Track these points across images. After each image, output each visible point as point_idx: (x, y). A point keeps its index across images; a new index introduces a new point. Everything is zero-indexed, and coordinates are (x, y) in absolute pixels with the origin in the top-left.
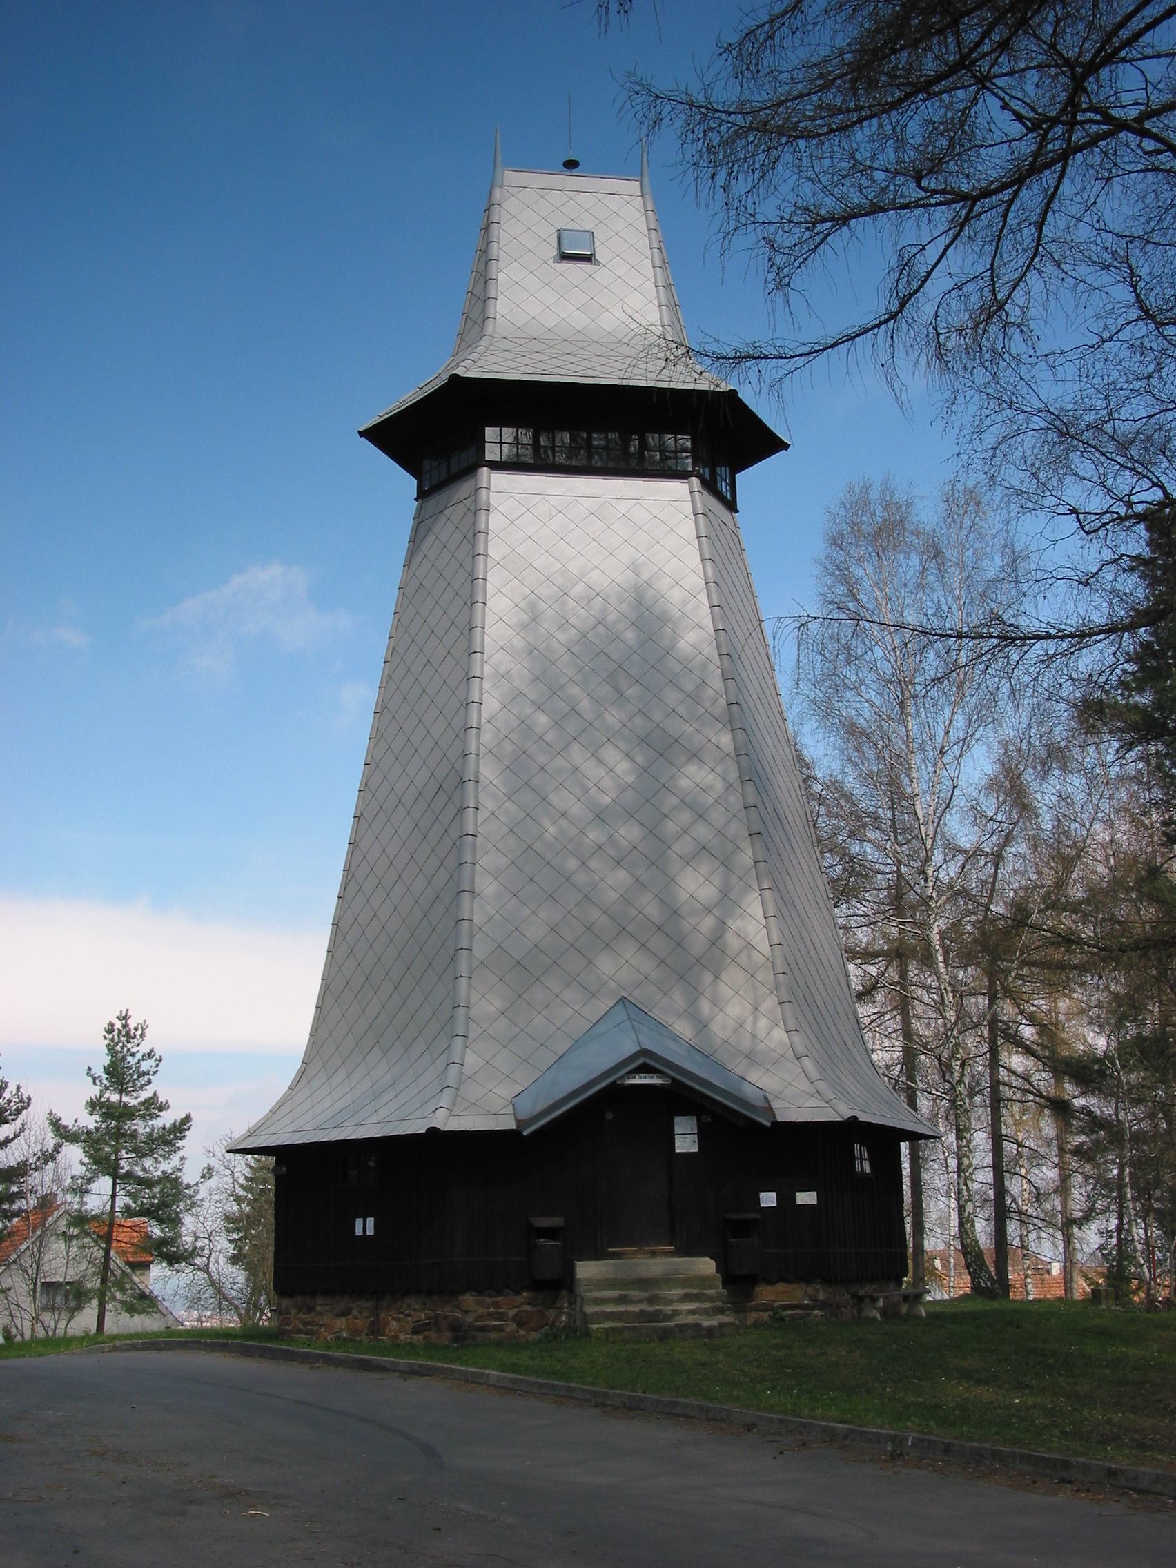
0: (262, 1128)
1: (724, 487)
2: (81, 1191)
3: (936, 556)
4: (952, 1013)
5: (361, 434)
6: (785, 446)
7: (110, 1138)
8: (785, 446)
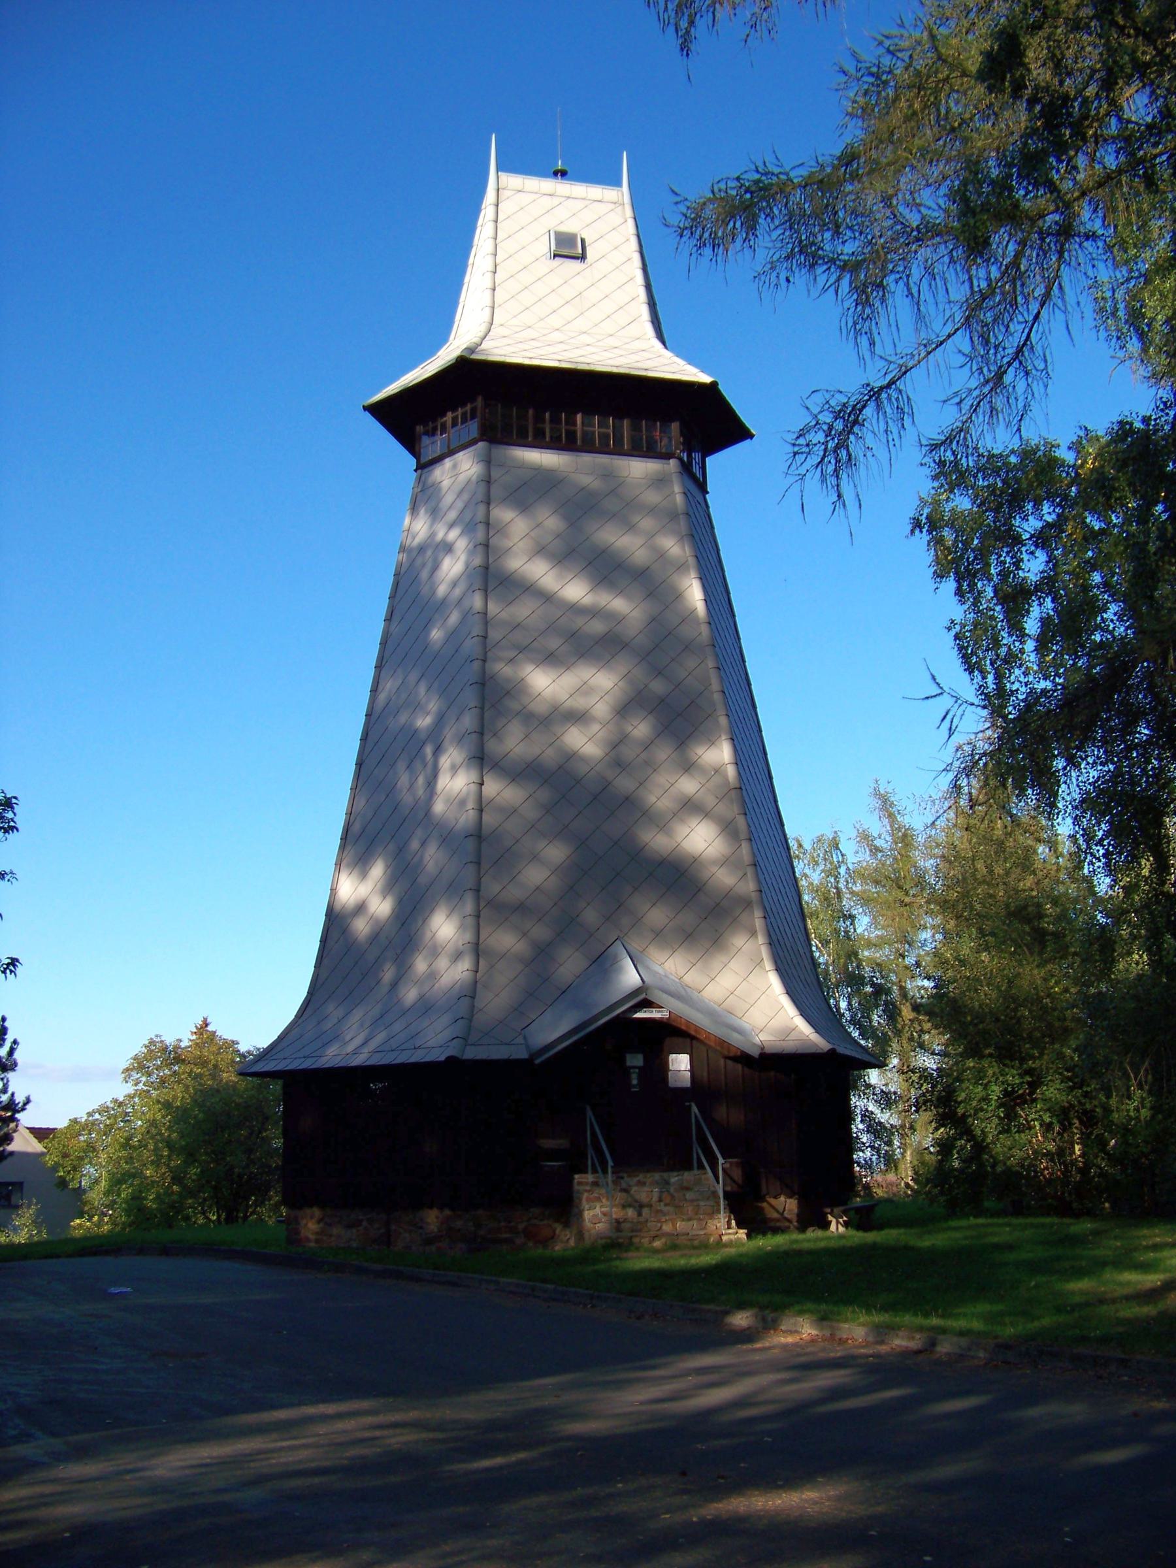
0: (269, 1055)
1: (696, 470)
2: (984, 585)
3: (94, 1150)
4: (821, 960)
5: (365, 408)
6: (751, 436)
7: (1083, 835)
8: (751, 436)
